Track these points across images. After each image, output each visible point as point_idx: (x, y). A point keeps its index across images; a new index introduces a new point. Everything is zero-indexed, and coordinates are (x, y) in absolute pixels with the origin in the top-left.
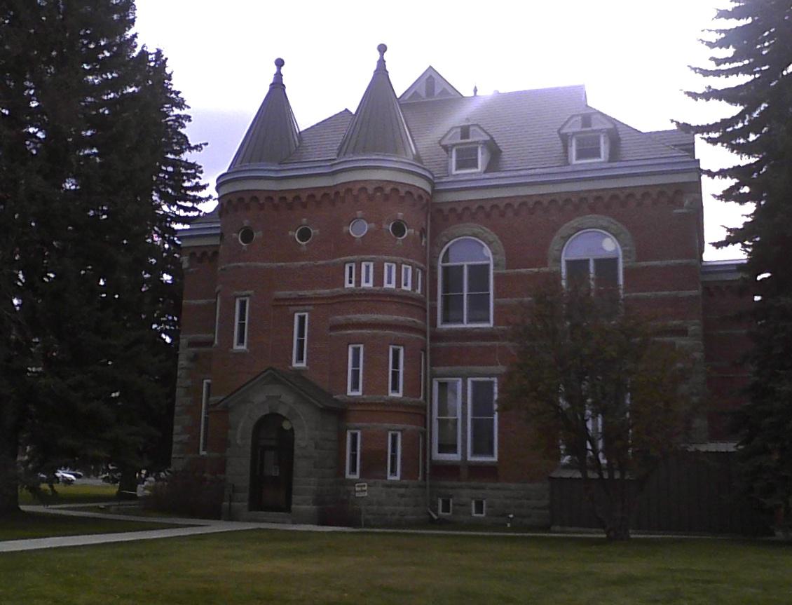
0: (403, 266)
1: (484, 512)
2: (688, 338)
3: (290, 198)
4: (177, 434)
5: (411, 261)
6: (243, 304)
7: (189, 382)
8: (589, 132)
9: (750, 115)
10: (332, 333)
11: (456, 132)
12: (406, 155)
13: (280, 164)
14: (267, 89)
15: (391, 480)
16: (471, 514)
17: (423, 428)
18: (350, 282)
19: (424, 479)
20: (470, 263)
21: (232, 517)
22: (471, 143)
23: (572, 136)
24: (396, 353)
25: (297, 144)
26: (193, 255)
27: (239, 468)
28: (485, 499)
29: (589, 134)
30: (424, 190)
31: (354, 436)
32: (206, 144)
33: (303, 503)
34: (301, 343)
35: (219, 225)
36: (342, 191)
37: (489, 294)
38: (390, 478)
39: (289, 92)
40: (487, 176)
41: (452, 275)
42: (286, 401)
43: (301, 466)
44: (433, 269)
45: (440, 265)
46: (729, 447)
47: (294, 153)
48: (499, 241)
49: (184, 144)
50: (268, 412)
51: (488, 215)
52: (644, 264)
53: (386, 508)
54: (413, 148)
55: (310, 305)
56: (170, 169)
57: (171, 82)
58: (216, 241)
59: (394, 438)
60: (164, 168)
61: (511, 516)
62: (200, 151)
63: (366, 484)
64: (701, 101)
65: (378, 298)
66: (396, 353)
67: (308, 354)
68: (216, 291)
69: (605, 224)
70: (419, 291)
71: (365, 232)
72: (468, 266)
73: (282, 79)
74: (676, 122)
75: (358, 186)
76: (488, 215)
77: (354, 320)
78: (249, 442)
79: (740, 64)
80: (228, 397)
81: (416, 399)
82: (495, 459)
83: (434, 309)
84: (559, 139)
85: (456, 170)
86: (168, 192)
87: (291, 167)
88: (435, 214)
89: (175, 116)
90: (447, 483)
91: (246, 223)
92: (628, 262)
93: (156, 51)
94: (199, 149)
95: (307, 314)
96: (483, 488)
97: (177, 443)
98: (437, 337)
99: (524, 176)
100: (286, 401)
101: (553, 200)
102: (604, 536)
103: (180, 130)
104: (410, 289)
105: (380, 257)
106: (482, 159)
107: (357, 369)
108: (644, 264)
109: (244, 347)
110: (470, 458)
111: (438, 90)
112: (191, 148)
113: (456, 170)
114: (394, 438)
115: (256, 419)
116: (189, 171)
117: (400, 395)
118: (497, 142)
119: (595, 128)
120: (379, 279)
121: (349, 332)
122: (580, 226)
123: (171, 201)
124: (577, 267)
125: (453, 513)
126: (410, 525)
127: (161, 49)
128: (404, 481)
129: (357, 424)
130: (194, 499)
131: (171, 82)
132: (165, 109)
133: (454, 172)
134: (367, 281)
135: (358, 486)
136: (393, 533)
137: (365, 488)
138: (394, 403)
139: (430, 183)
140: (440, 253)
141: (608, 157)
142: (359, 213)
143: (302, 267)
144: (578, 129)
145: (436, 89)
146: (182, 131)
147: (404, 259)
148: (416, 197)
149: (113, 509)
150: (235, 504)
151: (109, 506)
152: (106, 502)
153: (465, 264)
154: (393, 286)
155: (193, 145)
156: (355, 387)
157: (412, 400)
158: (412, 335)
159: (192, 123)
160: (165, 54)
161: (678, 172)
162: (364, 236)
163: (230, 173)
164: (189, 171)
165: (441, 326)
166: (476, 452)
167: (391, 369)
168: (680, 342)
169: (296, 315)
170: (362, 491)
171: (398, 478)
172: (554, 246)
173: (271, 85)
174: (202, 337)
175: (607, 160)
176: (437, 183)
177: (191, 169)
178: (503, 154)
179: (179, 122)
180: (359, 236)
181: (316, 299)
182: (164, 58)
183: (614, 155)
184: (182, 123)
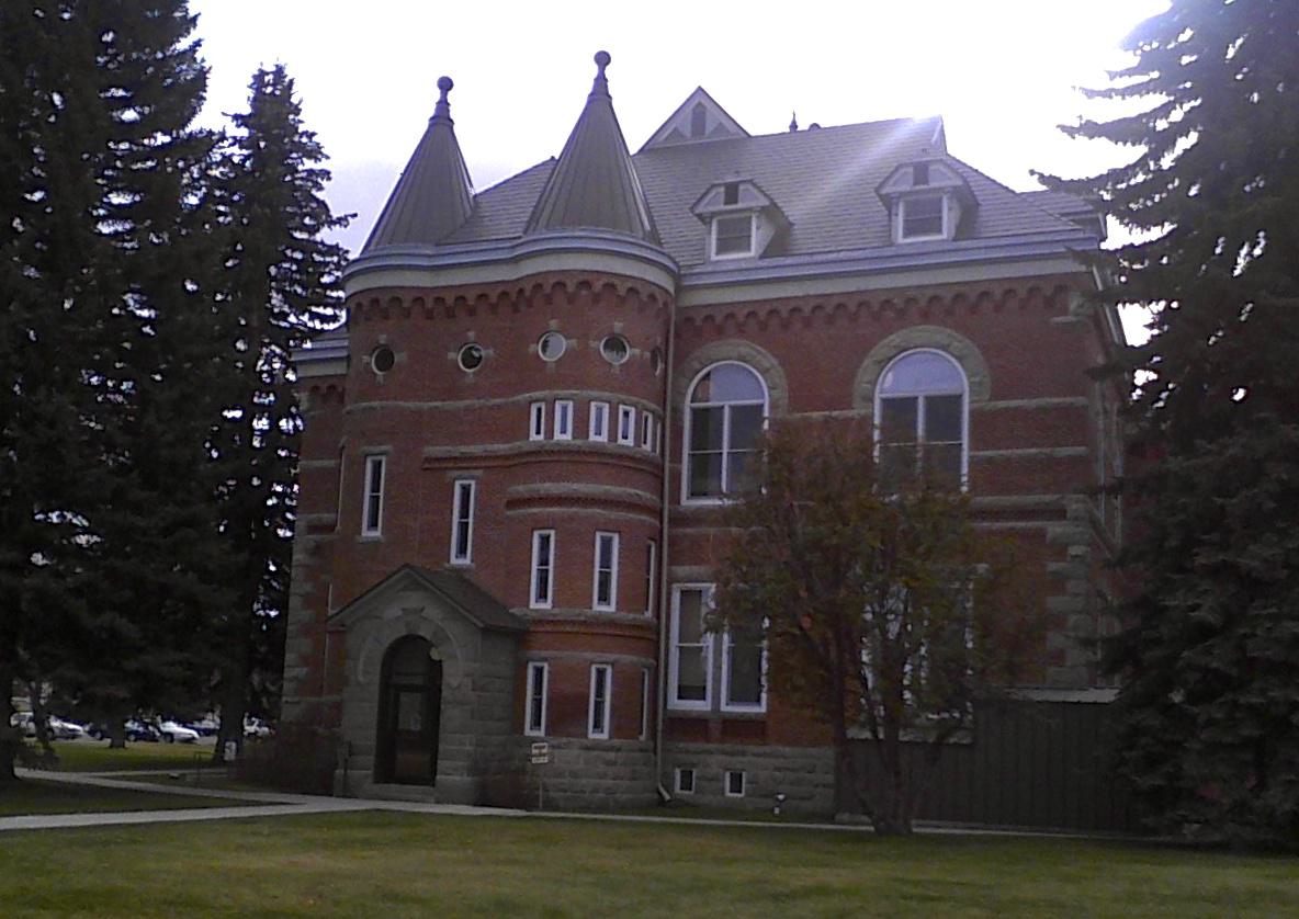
0: (621, 407)
1: (743, 790)
2: (1065, 522)
3: (450, 299)
4: (289, 666)
5: (635, 399)
6: (377, 466)
7: (308, 587)
8: (924, 191)
9: (1157, 160)
10: (509, 513)
11: (906, 173)
12: (632, 232)
13: (437, 245)
14: (424, 126)
15: (594, 740)
16: (723, 793)
17: (652, 661)
18: (538, 433)
19: (653, 735)
20: (733, 403)
21: (347, 794)
22: (929, 191)
23: (899, 198)
24: (607, 544)
25: (469, 213)
26: (315, 389)
27: (360, 721)
28: (743, 770)
29: (930, 195)
30: (658, 286)
31: (539, 671)
32: (355, 215)
33: (452, 773)
34: (464, 527)
35: (346, 344)
36: (528, 288)
37: (721, 454)
38: (592, 735)
39: (459, 130)
40: (765, 263)
41: (705, 421)
42: (431, 617)
43: (451, 716)
44: (677, 412)
45: (688, 406)
46: (1107, 695)
47: (462, 227)
48: (780, 368)
49: (322, 215)
50: (404, 633)
51: (763, 326)
52: (1002, 404)
53: (584, 781)
54: (646, 223)
55: (476, 468)
56: (298, 255)
57: (300, 117)
58: (340, 369)
59: (601, 673)
60: (289, 252)
61: (781, 797)
62: (345, 226)
63: (545, 744)
64: (1081, 139)
65: (580, 458)
66: (607, 544)
67: (473, 546)
68: (340, 445)
69: (946, 341)
70: (647, 447)
71: (561, 355)
72: (733, 408)
73: (448, 111)
74: (1039, 173)
75: (552, 281)
76: (763, 326)
77: (542, 492)
78: (377, 679)
79: (1145, 79)
80: (341, 611)
81: (638, 616)
82: (763, 709)
83: (676, 477)
84: (880, 204)
85: (717, 254)
86: (295, 291)
87: (484, 247)
88: (685, 329)
89: (306, 171)
90: (692, 746)
91: (383, 339)
92: (976, 401)
93: (274, 69)
94: (344, 223)
95: (473, 483)
96: (743, 754)
97: (291, 680)
98: (680, 519)
99: (822, 263)
100: (431, 617)
101: (863, 301)
102: (872, 829)
103: (314, 192)
104: (632, 444)
105: (584, 393)
106: (949, 218)
107: (544, 567)
108: (1002, 404)
109: (377, 534)
110: (724, 708)
111: (709, 128)
112: (332, 223)
113: (717, 254)
114: (601, 673)
115: (387, 643)
116: (328, 259)
117: (611, 608)
118: (780, 205)
119: (933, 185)
120: (581, 428)
121: (535, 510)
122: (903, 344)
123: (301, 306)
124: (899, 409)
125: (696, 792)
126: (623, 808)
127: (282, 64)
128: (616, 740)
129: (544, 654)
130: (300, 765)
131: (300, 117)
132: (290, 161)
133: (714, 258)
134: (563, 431)
135: (536, 748)
136: (562, 818)
137: (545, 751)
138: (610, 622)
139: (672, 276)
140: (688, 386)
141: (953, 232)
142: (553, 324)
143: (467, 409)
144: (905, 188)
145: (707, 126)
146: (319, 195)
147: (623, 397)
148: (644, 297)
149: (188, 779)
150: (355, 773)
151: (184, 775)
152: (181, 769)
153: (727, 404)
154: (604, 438)
155: (335, 215)
156: (542, 595)
157: (631, 616)
158: (631, 515)
159: (333, 181)
160: (289, 73)
161: (1036, 258)
162: (560, 359)
163: (365, 259)
164: (328, 259)
165: (687, 502)
166: (734, 698)
167: (597, 569)
168: (1054, 529)
169: (458, 484)
170: (541, 755)
171: (605, 736)
172: (862, 378)
173: (432, 119)
174: (327, 517)
175: (757, 256)
176: (685, 275)
177: (332, 255)
178: (980, 208)
179: (312, 181)
180: (553, 360)
181: (485, 458)
182: (287, 80)
183: (968, 224)
184: (317, 183)
